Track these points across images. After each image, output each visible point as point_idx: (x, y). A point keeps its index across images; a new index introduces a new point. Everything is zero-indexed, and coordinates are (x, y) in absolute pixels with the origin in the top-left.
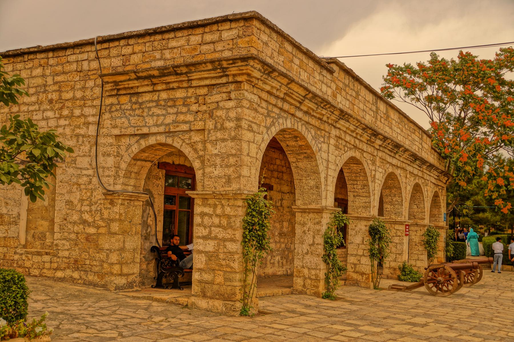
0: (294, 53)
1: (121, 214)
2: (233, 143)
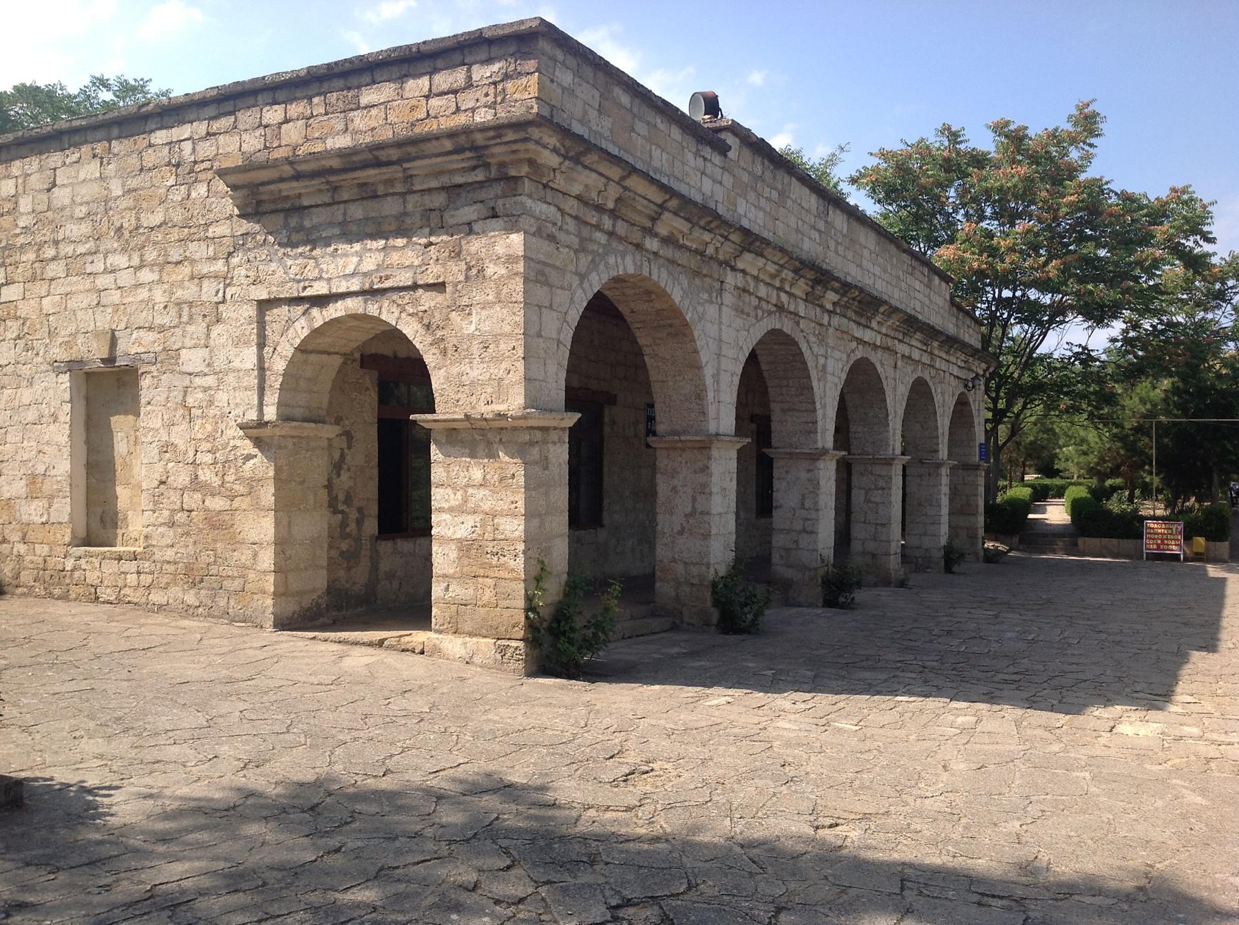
2: (505, 311)
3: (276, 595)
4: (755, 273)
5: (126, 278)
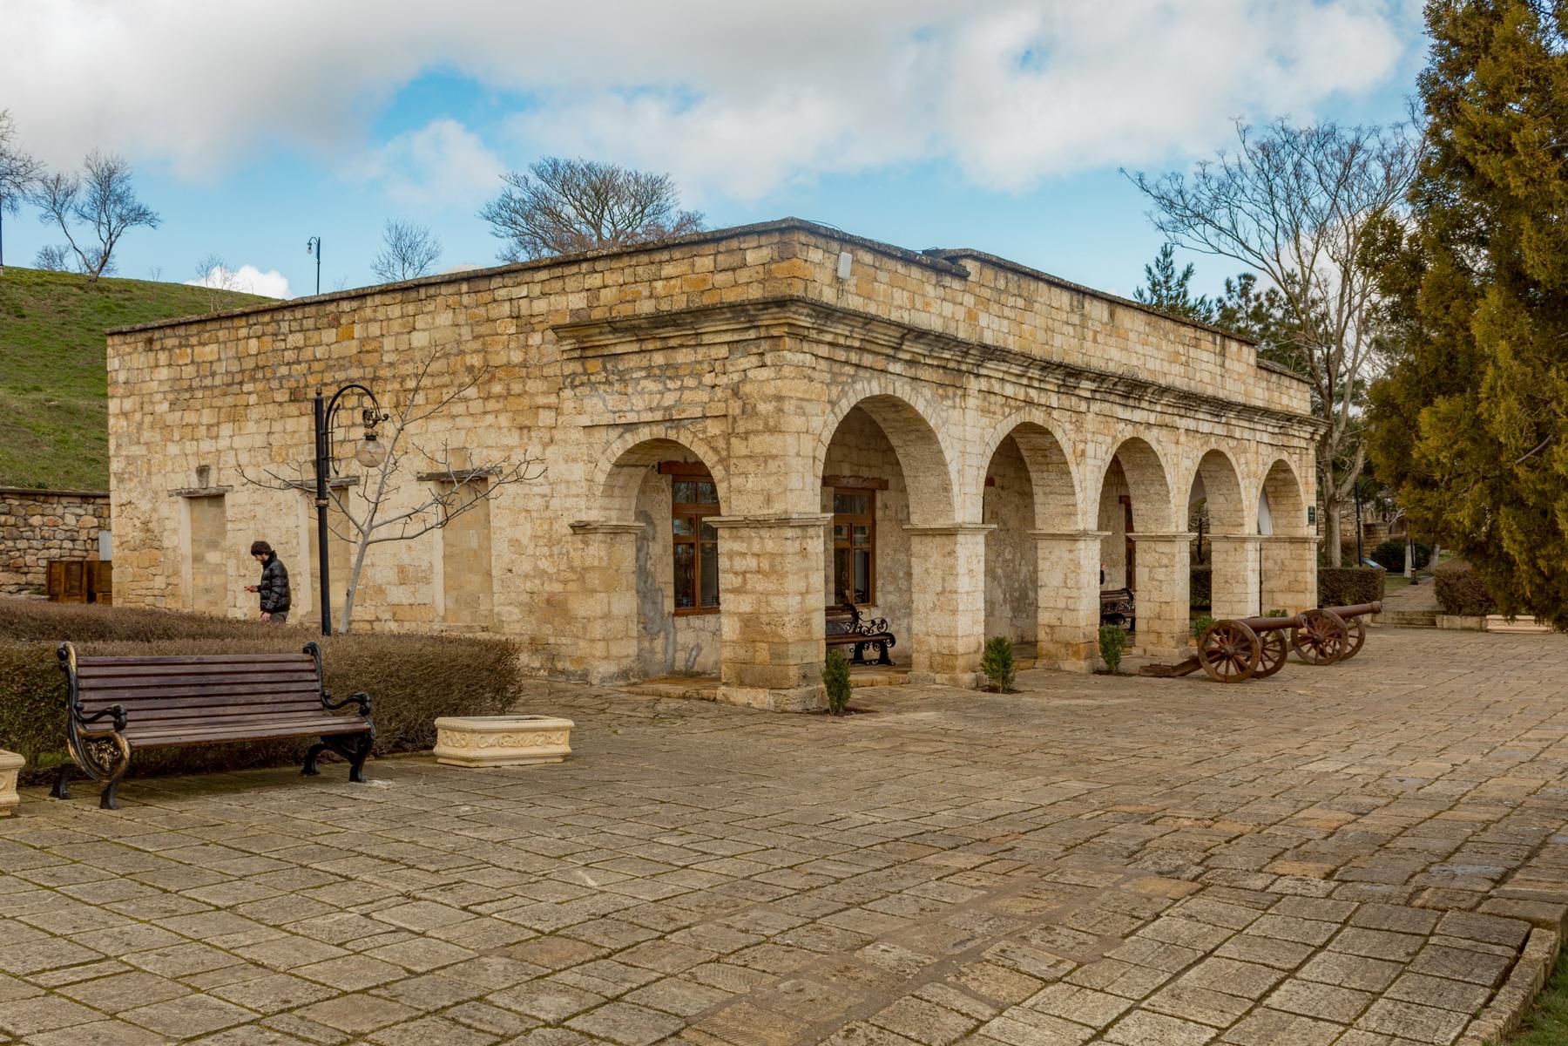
0: (877, 264)
1: (601, 559)
5: (476, 406)
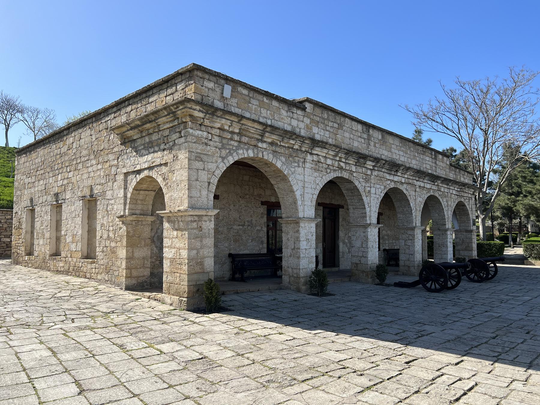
3: (126, 277)
4: (324, 155)
